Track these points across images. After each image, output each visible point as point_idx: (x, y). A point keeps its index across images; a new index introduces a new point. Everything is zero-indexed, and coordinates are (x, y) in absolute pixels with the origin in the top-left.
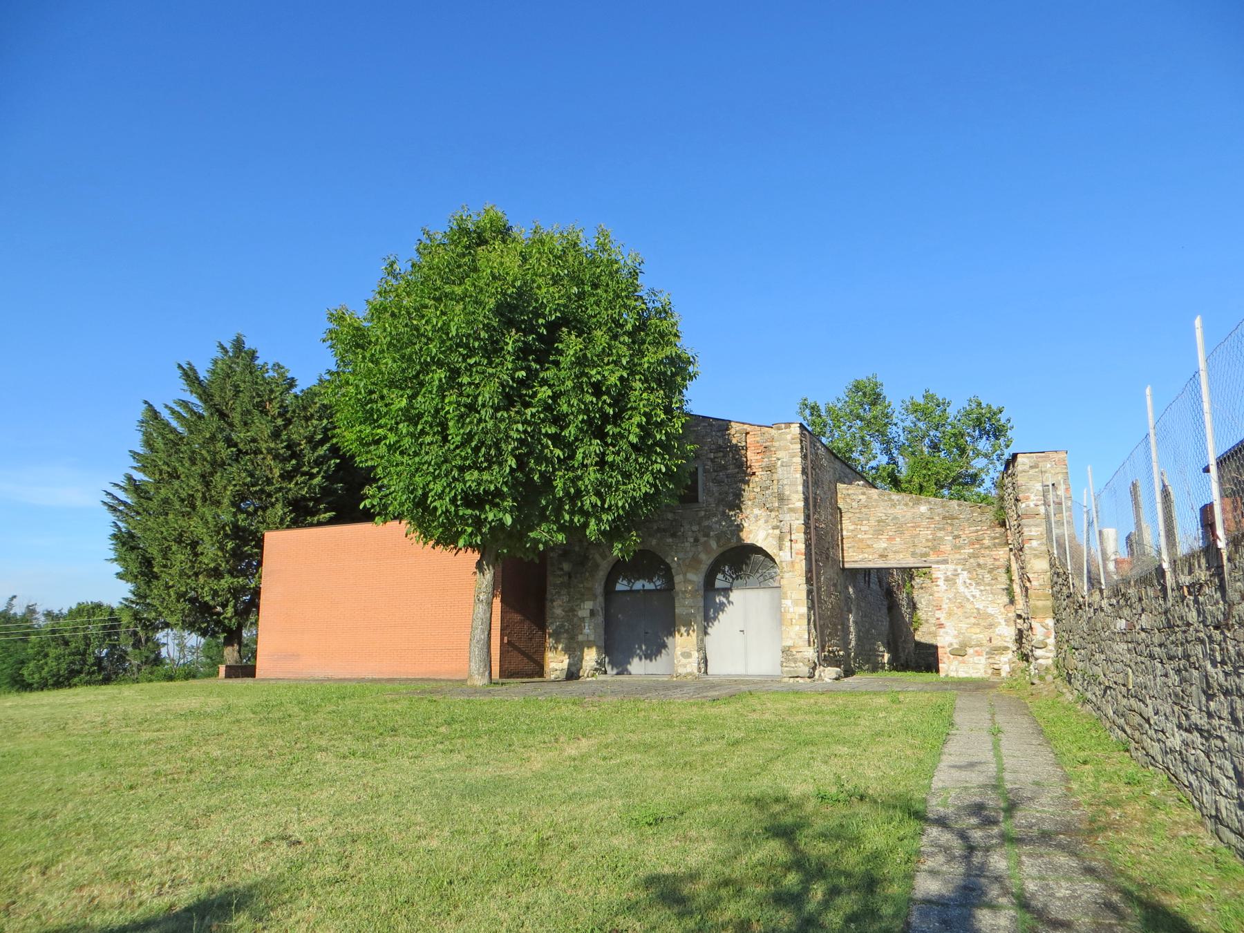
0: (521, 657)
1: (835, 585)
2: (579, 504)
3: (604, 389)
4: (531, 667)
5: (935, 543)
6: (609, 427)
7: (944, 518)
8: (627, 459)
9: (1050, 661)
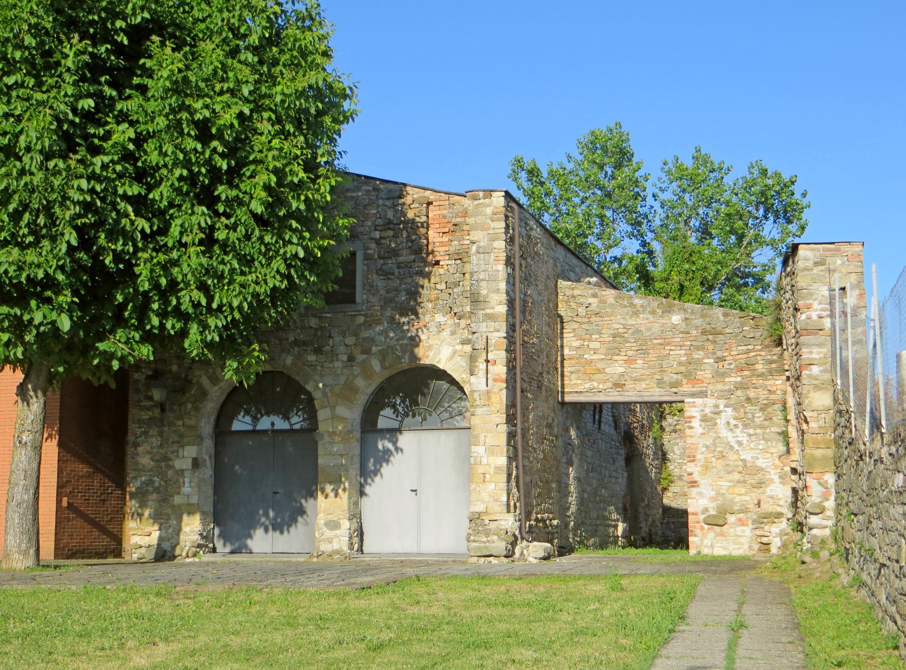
0: (88, 527)
1: (549, 426)
2: (174, 302)
3: (214, 131)
4: (105, 542)
5: (691, 367)
6: (221, 188)
7: (704, 332)
8: (248, 237)
9: (827, 532)
